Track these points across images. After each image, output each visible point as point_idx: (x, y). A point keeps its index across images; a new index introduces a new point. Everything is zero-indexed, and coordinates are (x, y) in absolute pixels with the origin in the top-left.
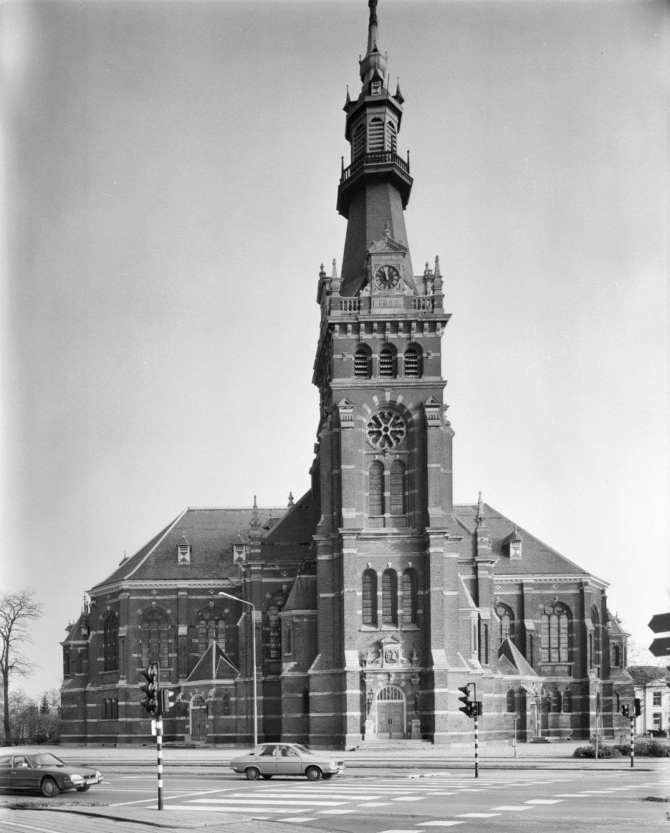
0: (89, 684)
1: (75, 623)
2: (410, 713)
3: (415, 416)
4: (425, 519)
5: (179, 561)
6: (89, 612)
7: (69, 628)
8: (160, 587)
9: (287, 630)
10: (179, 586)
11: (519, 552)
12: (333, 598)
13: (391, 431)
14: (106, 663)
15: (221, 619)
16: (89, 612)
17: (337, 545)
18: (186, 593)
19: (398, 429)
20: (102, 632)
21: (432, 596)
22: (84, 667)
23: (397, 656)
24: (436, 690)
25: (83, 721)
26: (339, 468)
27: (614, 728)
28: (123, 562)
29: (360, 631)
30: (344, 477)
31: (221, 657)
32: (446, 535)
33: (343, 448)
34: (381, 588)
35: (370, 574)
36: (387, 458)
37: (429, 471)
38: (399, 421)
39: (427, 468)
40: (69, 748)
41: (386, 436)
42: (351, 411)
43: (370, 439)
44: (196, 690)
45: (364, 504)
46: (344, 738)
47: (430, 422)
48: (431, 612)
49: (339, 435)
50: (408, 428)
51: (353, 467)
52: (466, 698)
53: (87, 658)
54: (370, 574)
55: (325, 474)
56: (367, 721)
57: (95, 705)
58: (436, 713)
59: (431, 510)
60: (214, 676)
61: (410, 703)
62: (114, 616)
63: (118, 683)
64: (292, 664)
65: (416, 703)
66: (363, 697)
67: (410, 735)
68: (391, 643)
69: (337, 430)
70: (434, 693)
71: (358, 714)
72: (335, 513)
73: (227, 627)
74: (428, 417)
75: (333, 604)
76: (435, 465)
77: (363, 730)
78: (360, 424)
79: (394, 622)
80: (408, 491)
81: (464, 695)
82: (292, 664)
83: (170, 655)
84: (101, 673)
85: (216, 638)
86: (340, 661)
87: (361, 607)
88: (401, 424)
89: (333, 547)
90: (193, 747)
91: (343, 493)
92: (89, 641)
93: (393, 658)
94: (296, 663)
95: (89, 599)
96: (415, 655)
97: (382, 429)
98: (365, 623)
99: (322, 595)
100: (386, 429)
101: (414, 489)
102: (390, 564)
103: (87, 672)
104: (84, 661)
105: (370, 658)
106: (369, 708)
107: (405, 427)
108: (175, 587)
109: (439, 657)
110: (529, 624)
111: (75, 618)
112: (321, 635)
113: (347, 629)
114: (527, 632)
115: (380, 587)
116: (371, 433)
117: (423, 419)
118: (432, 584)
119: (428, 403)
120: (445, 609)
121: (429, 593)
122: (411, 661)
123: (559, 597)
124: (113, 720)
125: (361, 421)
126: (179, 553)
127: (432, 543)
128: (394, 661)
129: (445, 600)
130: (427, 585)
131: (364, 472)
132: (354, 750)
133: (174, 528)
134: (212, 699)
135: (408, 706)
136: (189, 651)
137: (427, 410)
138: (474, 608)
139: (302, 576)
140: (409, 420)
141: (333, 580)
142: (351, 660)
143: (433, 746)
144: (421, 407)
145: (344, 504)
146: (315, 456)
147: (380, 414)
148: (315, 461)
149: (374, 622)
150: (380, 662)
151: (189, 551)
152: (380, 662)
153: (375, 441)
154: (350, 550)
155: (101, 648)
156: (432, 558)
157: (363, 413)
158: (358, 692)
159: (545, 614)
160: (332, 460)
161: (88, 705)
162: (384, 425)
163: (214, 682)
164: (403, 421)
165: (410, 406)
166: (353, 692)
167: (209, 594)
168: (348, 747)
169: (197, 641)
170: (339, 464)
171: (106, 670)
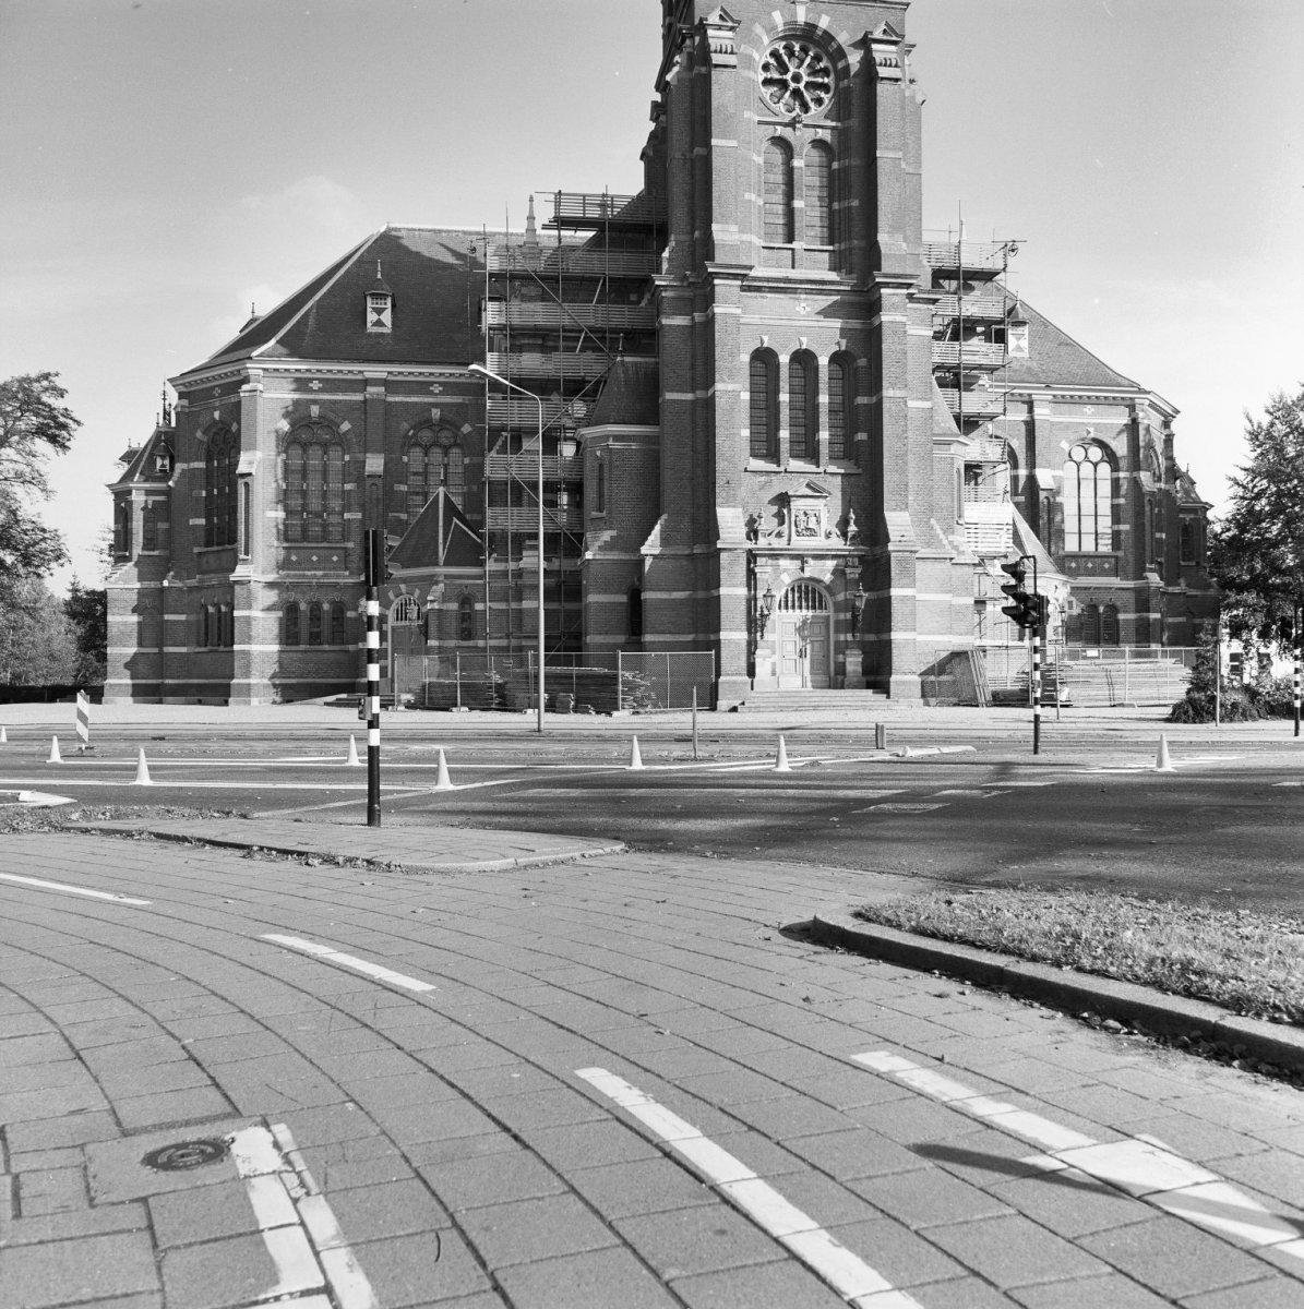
0: (172, 573)
1: (142, 446)
2: (842, 637)
3: (854, 58)
4: (873, 255)
5: (369, 325)
6: (173, 424)
7: (128, 457)
8: (329, 376)
9: (596, 464)
10: (368, 375)
11: (1024, 343)
12: (693, 402)
13: (807, 83)
14: (209, 529)
15: (456, 445)
16: (173, 424)
17: (700, 295)
18: (383, 389)
19: (820, 80)
20: (202, 465)
21: (886, 405)
22: (161, 538)
23: (818, 522)
24: (894, 592)
25: (156, 650)
26: (708, 147)
27: (252, 681)
28: (246, 326)
29: (746, 470)
30: (717, 162)
31: (455, 520)
32: (911, 291)
33: (714, 104)
34: (787, 387)
35: (764, 359)
36: (798, 133)
37: (880, 163)
38: (822, 65)
39: (876, 158)
40: (780, 859)
41: (797, 94)
42: (730, 34)
43: (767, 92)
44: (403, 586)
45: (755, 220)
46: (889, 642)
47: (883, 72)
48: (885, 438)
49: (707, 80)
50: (838, 80)
51: (734, 143)
52: (1015, 587)
53: (168, 520)
54: (764, 359)
55: (678, 155)
56: (758, 652)
57: (183, 617)
58: (895, 636)
59: (882, 238)
60: (441, 561)
61: (842, 616)
62: (229, 431)
63: (233, 571)
64: (606, 536)
65: (854, 616)
66: (751, 601)
67: (843, 681)
68: (807, 496)
69: (703, 70)
70: (890, 597)
71: (743, 636)
72: (697, 234)
73: (467, 461)
74: (878, 61)
75: (693, 414)
76: (891, 155)
77: (751, 672)
78: (748, 62)
79: (810, 452)
80: (840, 201)
81: (1013, 582)
82: (606, 536)
83: (346, 516)
84: (196, 550)
85: (445, 483)
86: (707, 529)
87: (747, 422)
88: (825, 72)
89: (692, 300)
90: (465, 233)
91: (715, 194)
92: (171, 483)
93: (810, 526)
94: (614, 533)
95: (173, 398)
96: (852, 522)
97: (788, 77)
98: (754, 455)
99: (669, 396)
100: (797, 78)
101: (848, 197)
102: (804, 340)
103: (164, 548)
104: (162, 526)
105: (767, 523)
106: (763, 626)
107: (832, 76)
108: (360, 377)
109: (897, 521)
110: (1044, 478)
111: (142, 436)
112: (667, 476)
113: (721, 465)
114: (1041, 492)
115: (784, 385)
116: (767, 82)
117: (869, 63)
118: (885, 384)
119: (878, 34)
120: (910, 434)
121: (879, 405)
122: (844, 534)
123: (1096, 430)
124: (222, 648)
125: (750, 58)
126: (369, 310)
127: (885, 303)
128: (812, 532)
129: (909, 415)
130: (875, 386)
131: (755, 158)
132: (734, 709)
133: (358, 260)
134: (436, 606)
135: (837, 622)
136: (388, 508)
137: (875, 46)
138: (958, 436)
139: (627, 359)
140: (840, 65)
141: (693, 366)
142: (730, 521)
143: (888, 702)
144: (865, 43)
145: (716, 214)
146: (652, 126)
147: (785, 47)
148: (653, 136)
149: (773, 455)
150: (786, 533)
151: (389, 305)
152: (786, 533)
153: (805, 108)
154: (728, 304)
155: (198, 499)
156: (886, 332)
157: (755, 42)
158: (743, 591)
159: (1071, 460)
160: (693, 129)
161: (166, 617)
162: (792, 70)
163: (441, 570)
164: (829, 65)
165: (843, 38)
166: (732, 591)
167: (432, 393)
168: (723, 704)
169: (404, 488)
170: (707, 135)
171: (208, 544)
